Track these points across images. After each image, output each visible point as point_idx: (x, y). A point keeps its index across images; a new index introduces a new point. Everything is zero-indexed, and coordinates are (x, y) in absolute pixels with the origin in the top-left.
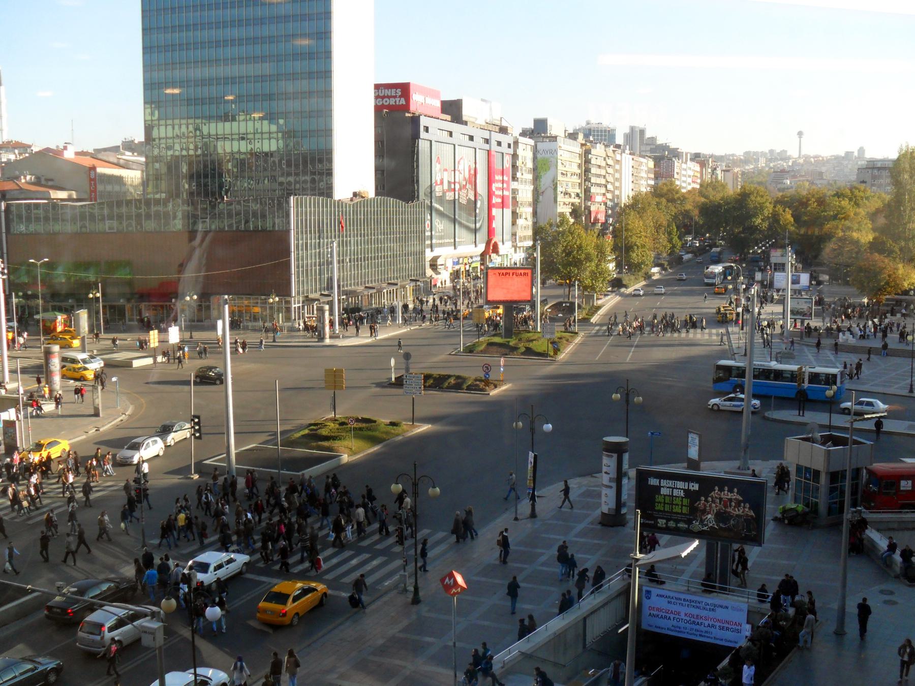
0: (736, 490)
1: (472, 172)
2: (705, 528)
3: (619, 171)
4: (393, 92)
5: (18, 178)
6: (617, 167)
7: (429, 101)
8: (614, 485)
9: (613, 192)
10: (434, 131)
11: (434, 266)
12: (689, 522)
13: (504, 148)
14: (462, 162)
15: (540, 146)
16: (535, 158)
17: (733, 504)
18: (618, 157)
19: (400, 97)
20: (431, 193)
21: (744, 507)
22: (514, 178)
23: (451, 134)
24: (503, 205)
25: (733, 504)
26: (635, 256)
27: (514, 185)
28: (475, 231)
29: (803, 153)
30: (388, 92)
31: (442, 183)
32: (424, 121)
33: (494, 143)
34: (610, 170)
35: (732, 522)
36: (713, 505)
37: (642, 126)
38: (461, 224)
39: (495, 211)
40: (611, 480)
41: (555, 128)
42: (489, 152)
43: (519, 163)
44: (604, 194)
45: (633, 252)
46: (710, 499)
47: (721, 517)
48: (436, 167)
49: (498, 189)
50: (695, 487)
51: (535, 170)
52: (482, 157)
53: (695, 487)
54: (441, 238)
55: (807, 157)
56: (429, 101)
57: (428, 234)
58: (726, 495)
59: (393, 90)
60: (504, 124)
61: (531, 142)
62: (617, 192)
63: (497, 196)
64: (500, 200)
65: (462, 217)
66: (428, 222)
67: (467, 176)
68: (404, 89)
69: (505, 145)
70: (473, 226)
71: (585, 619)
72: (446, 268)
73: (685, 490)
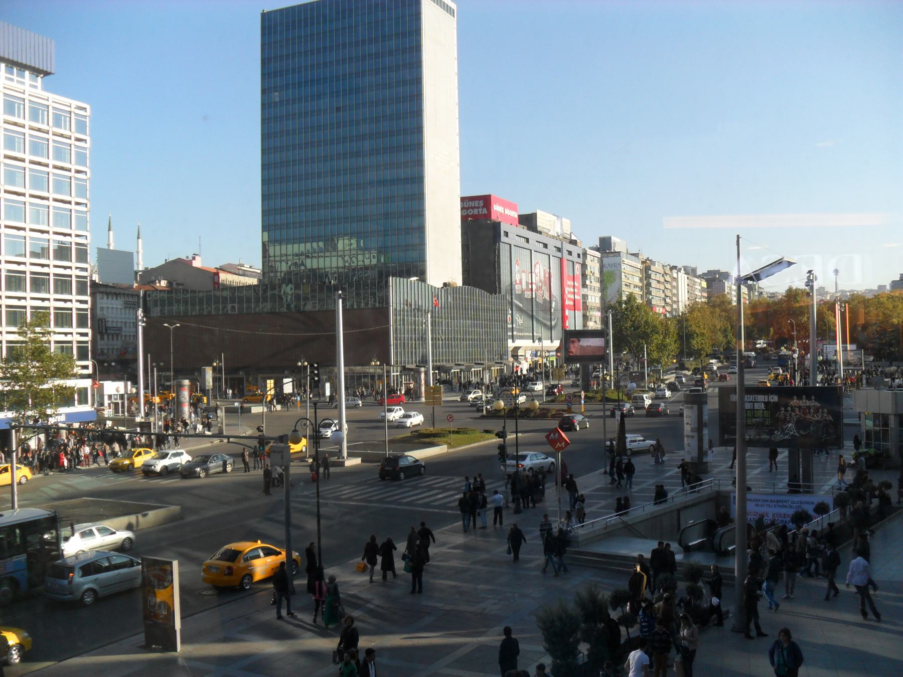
0: (813, 397)
1: (547, 276)
2: (787, 437)
3: (677, 288)
4: (476, 203)
5: (154, 282)
6: (674, 284)
7: (508, 212)
8: (696, 434)
9: (671, 306)
10: (513, 233)
11: (515, 356)
12: (771, 433)
13: (574, 258)
14: (538, 266)
15: (606, 260)
16: (601, 272)
17: (812, 411)
18: (675, 275)
19: (483, 207)
20: (511, 290)
21: (823, 413)
22: (584, 285)
23: (527, 240)
24: (574, 308)
25: (812, 411)
26: (695, 343)
27: (585, 291)
28: (551, 328)
29: (840, 288)
30: (472, 204)
31: (521, 283)
32: (504, 227)
33: (565, 253)
34: (668, 286)
35: (812, 428)
36: (793, 414)
37: (693, 266)
38: (537, 320)
39: (567, 312)
40: (692, 430)
41: (618, 244)
42: (561, 259)
43: (588, 272)
44: (664, 307)
45: (693, 339)
46: (789, 409)
47: (801, 424)
48: (516, 268)
49: (569, 292)
50: (775, 398)
51: (602, 281)
52: (555, 263)
53: (775, 398)
54: (520, 331)
55: (843, 292)
56: (508, 212)
57: (510, 326)
58: (804, 402)
59: (477, 202)
60: (573, 238)
61: (598, 254)
62: (675, 306)
63: (570, 299)
64: (572, 303)
65: (540, 315)
66: (509, 316)
67: (542, 279)
68: (486, 201)
69: (575, 254)
70: (549, 323)
71: (679, 511)
72: (526, 359)
73: (765, 403)
